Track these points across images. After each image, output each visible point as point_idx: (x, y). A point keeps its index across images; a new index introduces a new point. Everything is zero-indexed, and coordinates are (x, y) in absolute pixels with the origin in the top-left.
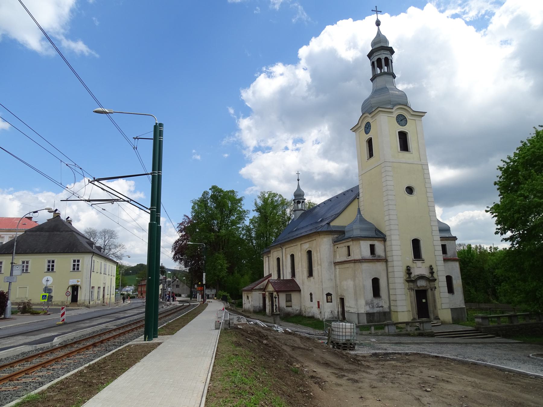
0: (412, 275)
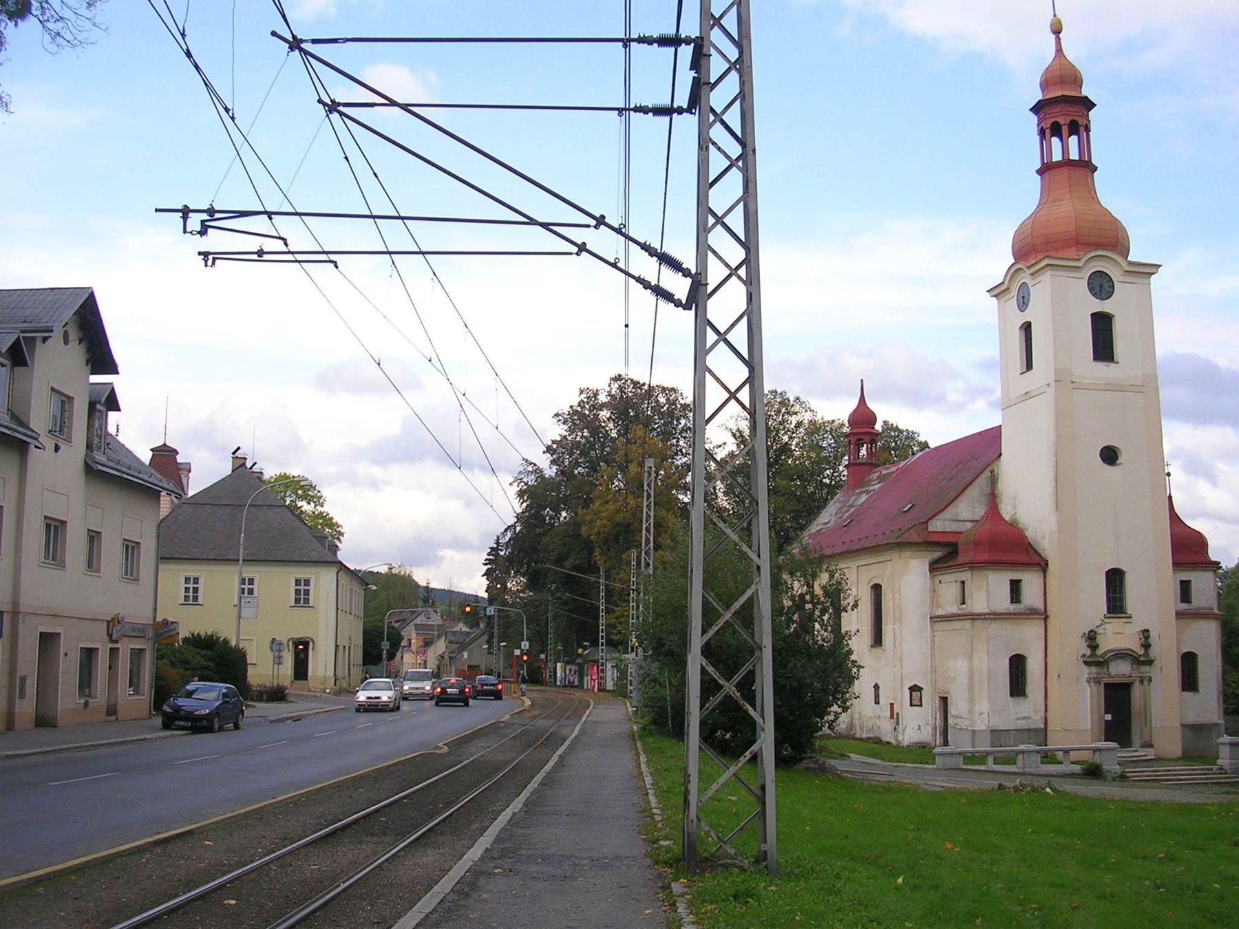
0: (1099, 652)
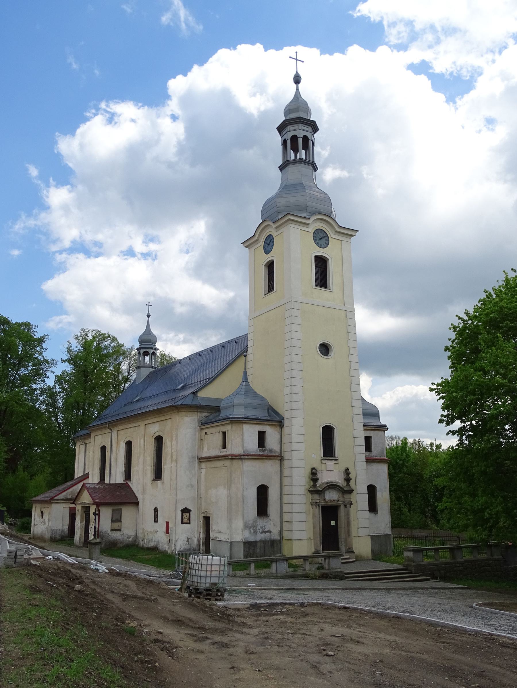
0: (319, 483)
